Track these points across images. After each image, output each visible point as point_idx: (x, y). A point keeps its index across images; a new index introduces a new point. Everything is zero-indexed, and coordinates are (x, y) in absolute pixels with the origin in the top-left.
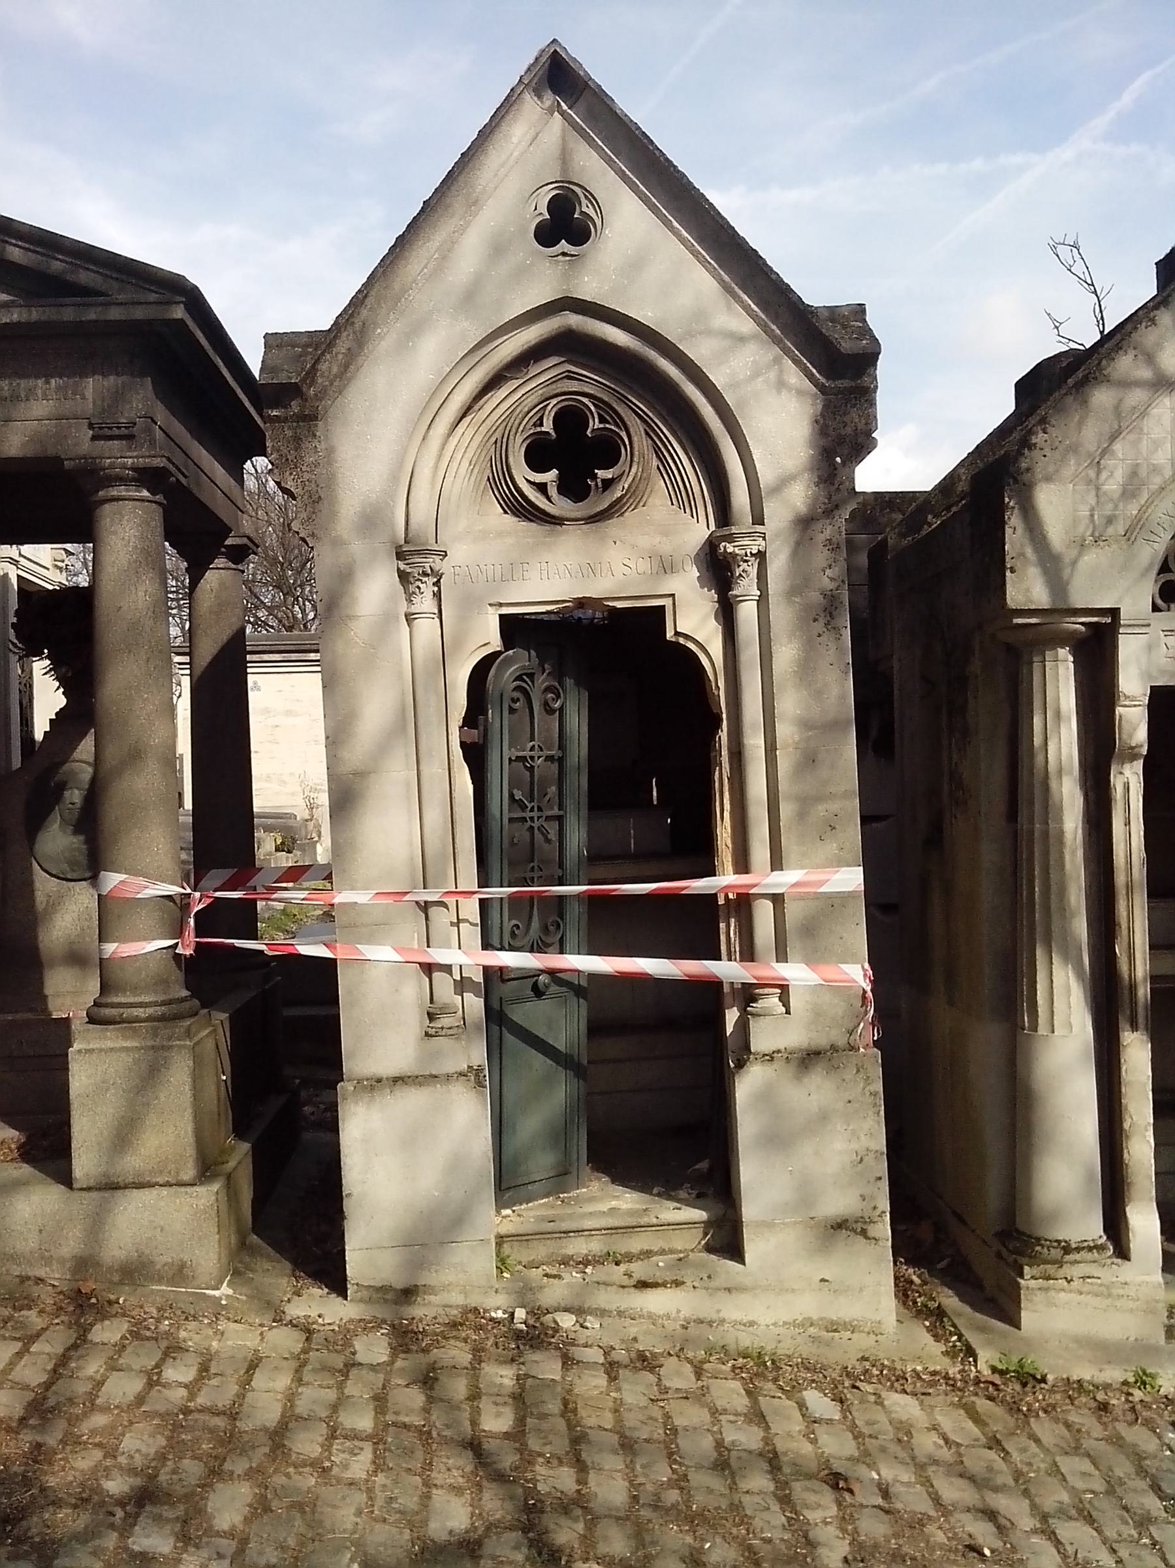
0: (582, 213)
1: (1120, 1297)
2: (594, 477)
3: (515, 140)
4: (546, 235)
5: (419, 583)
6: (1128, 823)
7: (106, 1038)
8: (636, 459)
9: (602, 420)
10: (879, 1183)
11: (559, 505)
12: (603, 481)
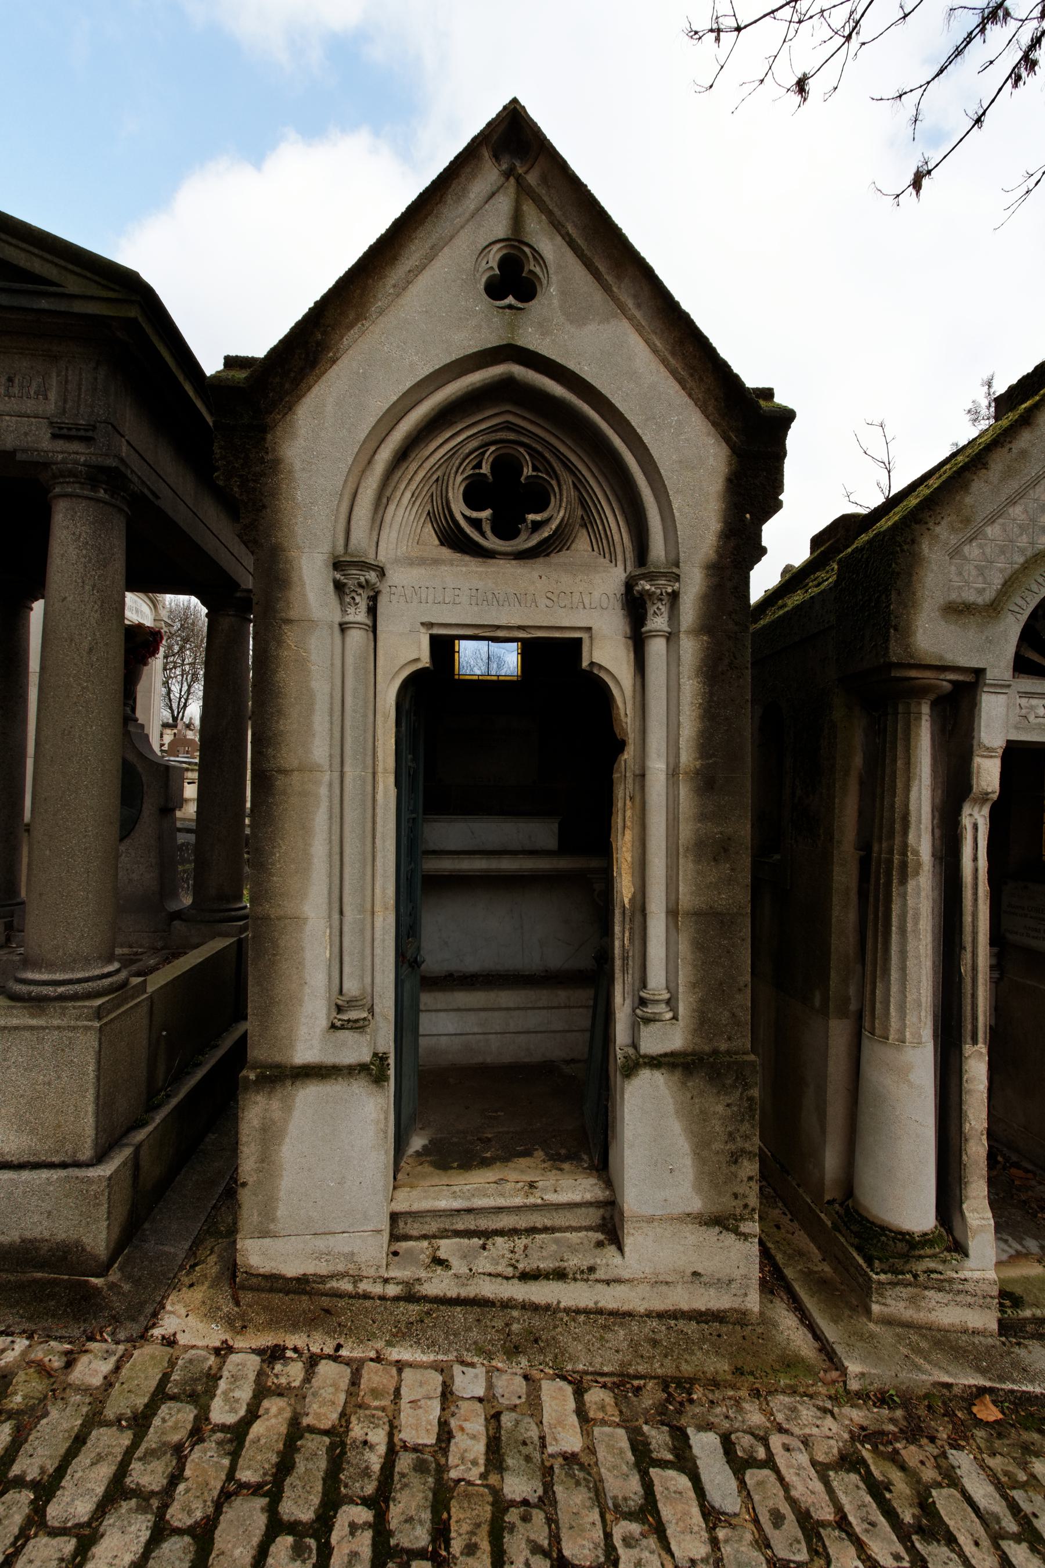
0: (531, 272)
1: (959, 1292)
2: (524, 520)
3: (472, 196)
4: (495, 289)
5: (353, 594)
6: (975, 859)
7: (12, 1016)
8: (564, 505)
9: (535, 469)
10: (752, 1184)
11: (492, 542)
12: (533, 522)
